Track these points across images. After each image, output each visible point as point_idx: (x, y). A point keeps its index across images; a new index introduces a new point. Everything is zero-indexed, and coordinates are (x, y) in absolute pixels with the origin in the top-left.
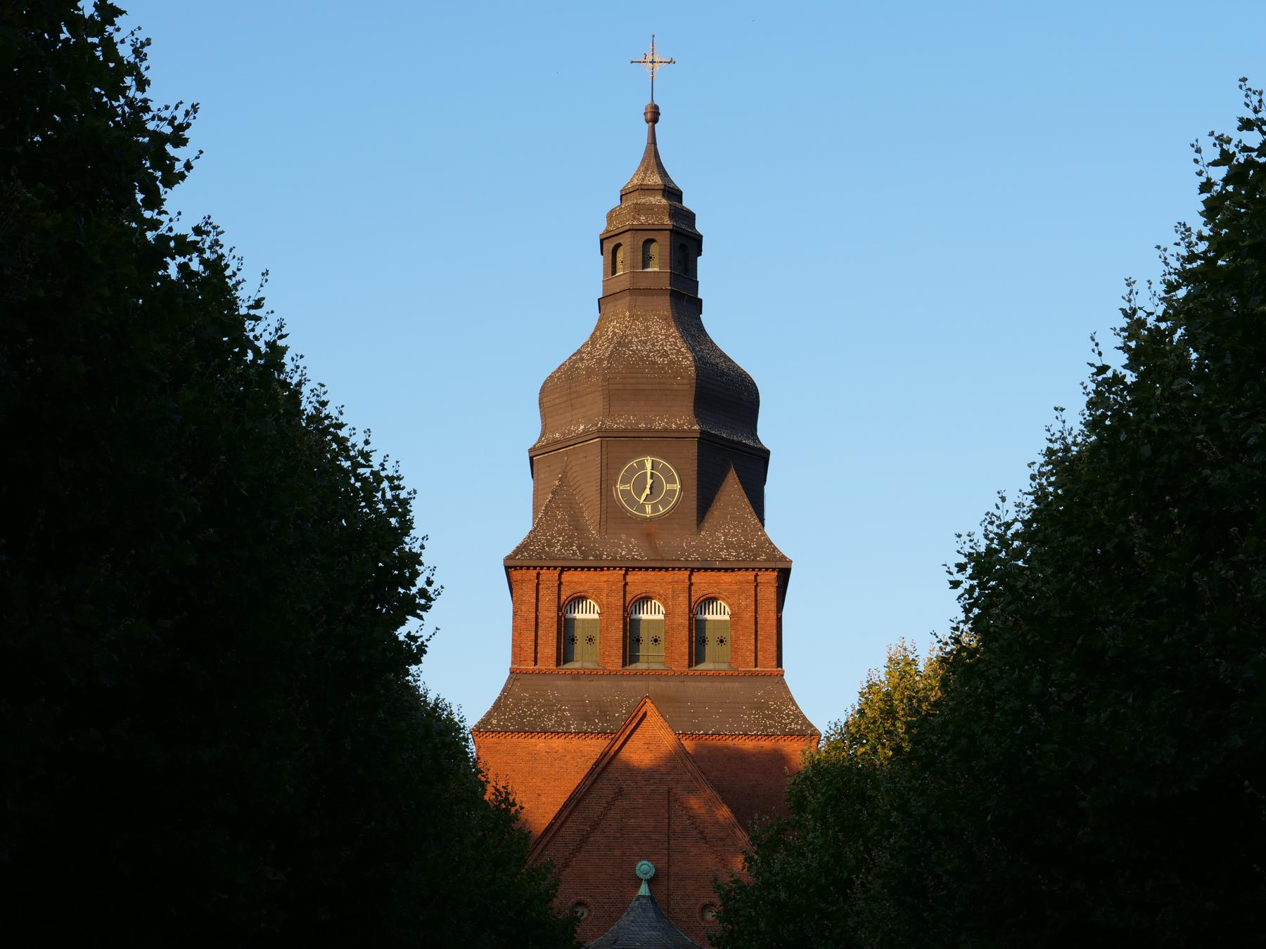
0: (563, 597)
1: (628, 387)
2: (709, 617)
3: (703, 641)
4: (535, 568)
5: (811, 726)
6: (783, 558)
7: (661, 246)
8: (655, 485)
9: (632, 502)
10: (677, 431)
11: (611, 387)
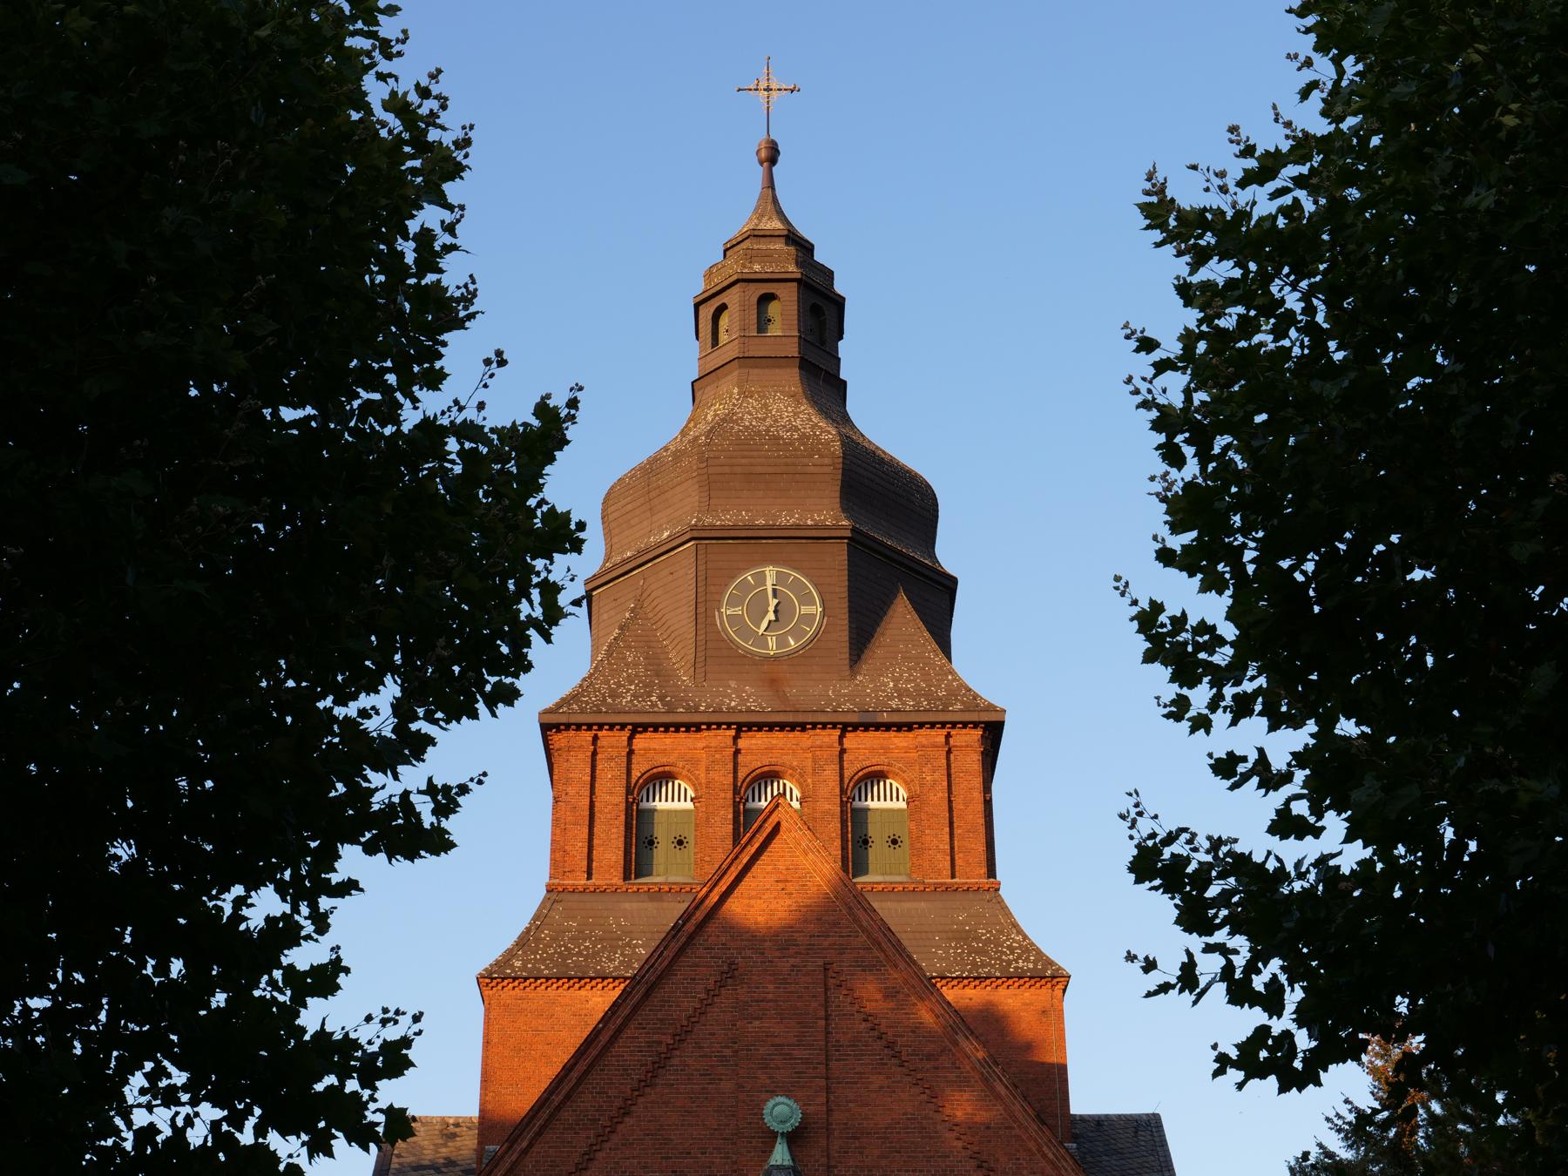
0: (636, 774)
1: (738, 470)
4: (590, 727)
5: (1051, 963)
6: (991, 708)
9: (746, 633)
10: (815, 527)
11: (711, 470)
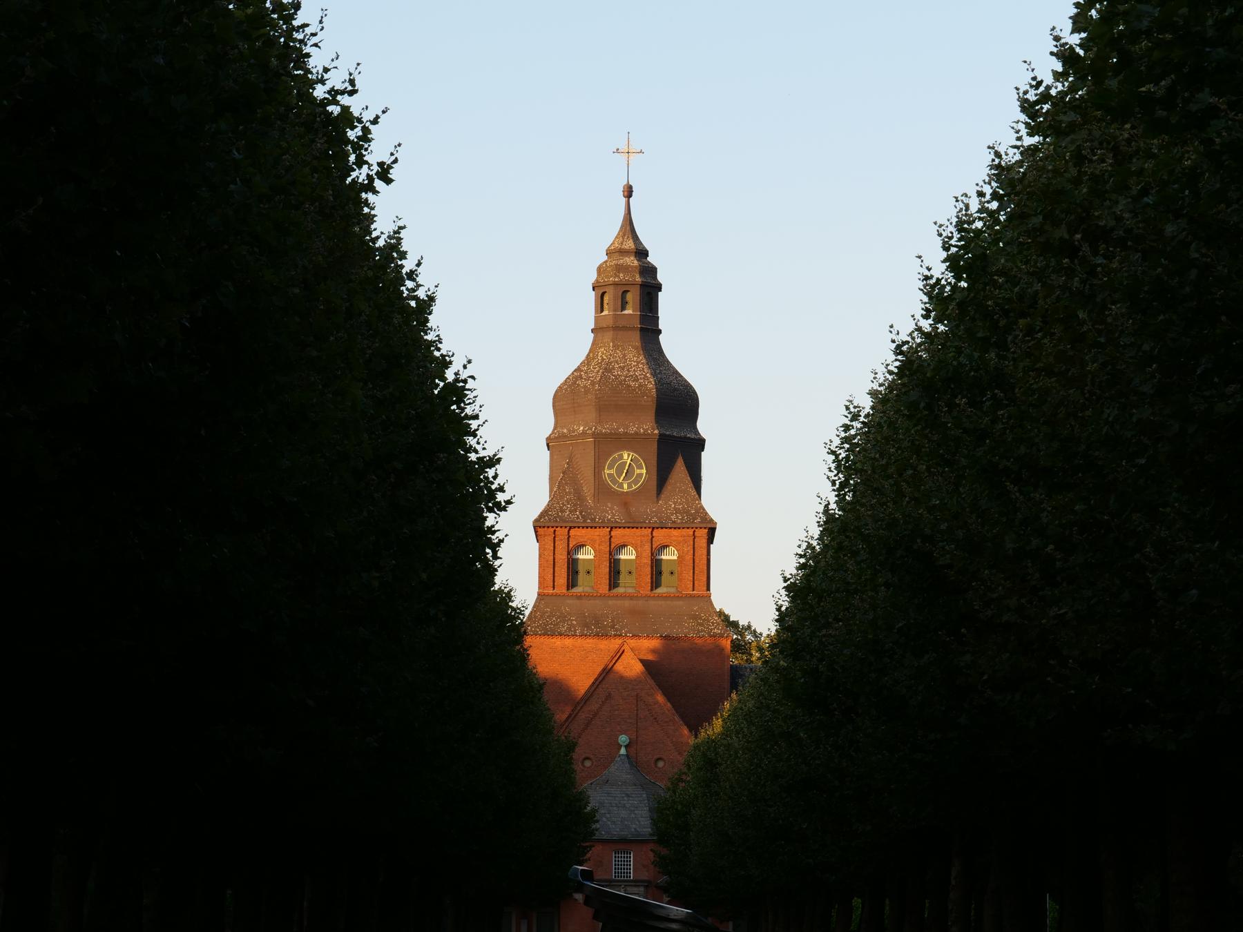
2: (664, 557)
3: (660, 573)
6: (712, 520)
7: (632, 292)
8: (630, 469)
9: (615, 481)
